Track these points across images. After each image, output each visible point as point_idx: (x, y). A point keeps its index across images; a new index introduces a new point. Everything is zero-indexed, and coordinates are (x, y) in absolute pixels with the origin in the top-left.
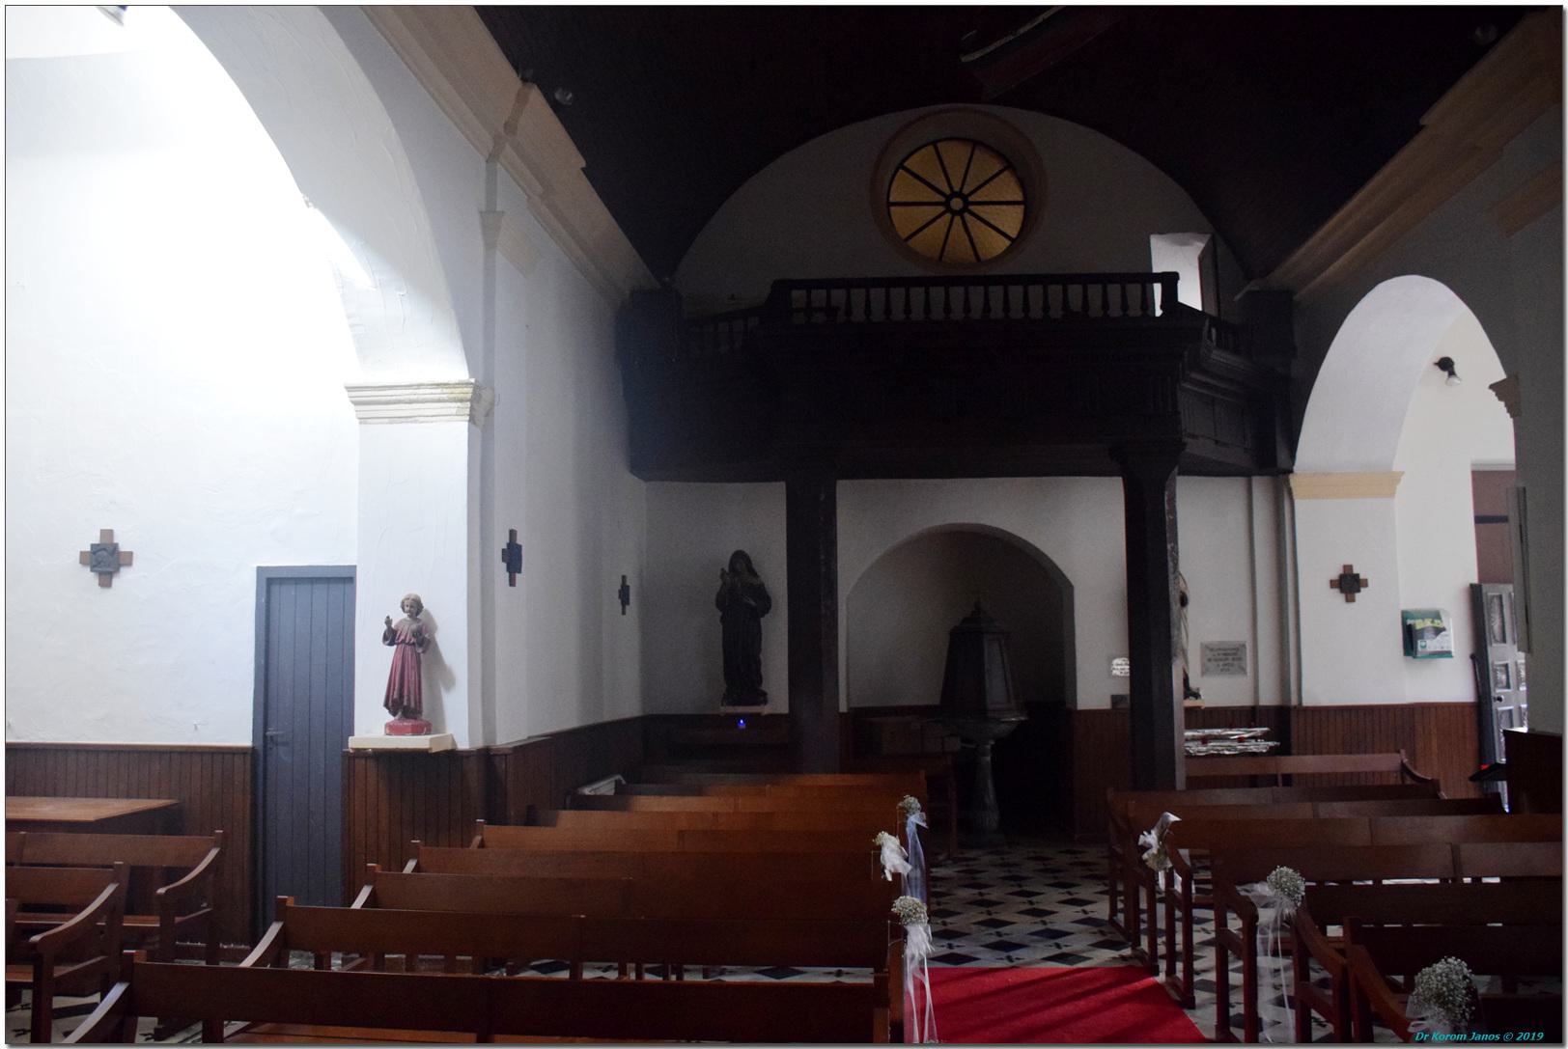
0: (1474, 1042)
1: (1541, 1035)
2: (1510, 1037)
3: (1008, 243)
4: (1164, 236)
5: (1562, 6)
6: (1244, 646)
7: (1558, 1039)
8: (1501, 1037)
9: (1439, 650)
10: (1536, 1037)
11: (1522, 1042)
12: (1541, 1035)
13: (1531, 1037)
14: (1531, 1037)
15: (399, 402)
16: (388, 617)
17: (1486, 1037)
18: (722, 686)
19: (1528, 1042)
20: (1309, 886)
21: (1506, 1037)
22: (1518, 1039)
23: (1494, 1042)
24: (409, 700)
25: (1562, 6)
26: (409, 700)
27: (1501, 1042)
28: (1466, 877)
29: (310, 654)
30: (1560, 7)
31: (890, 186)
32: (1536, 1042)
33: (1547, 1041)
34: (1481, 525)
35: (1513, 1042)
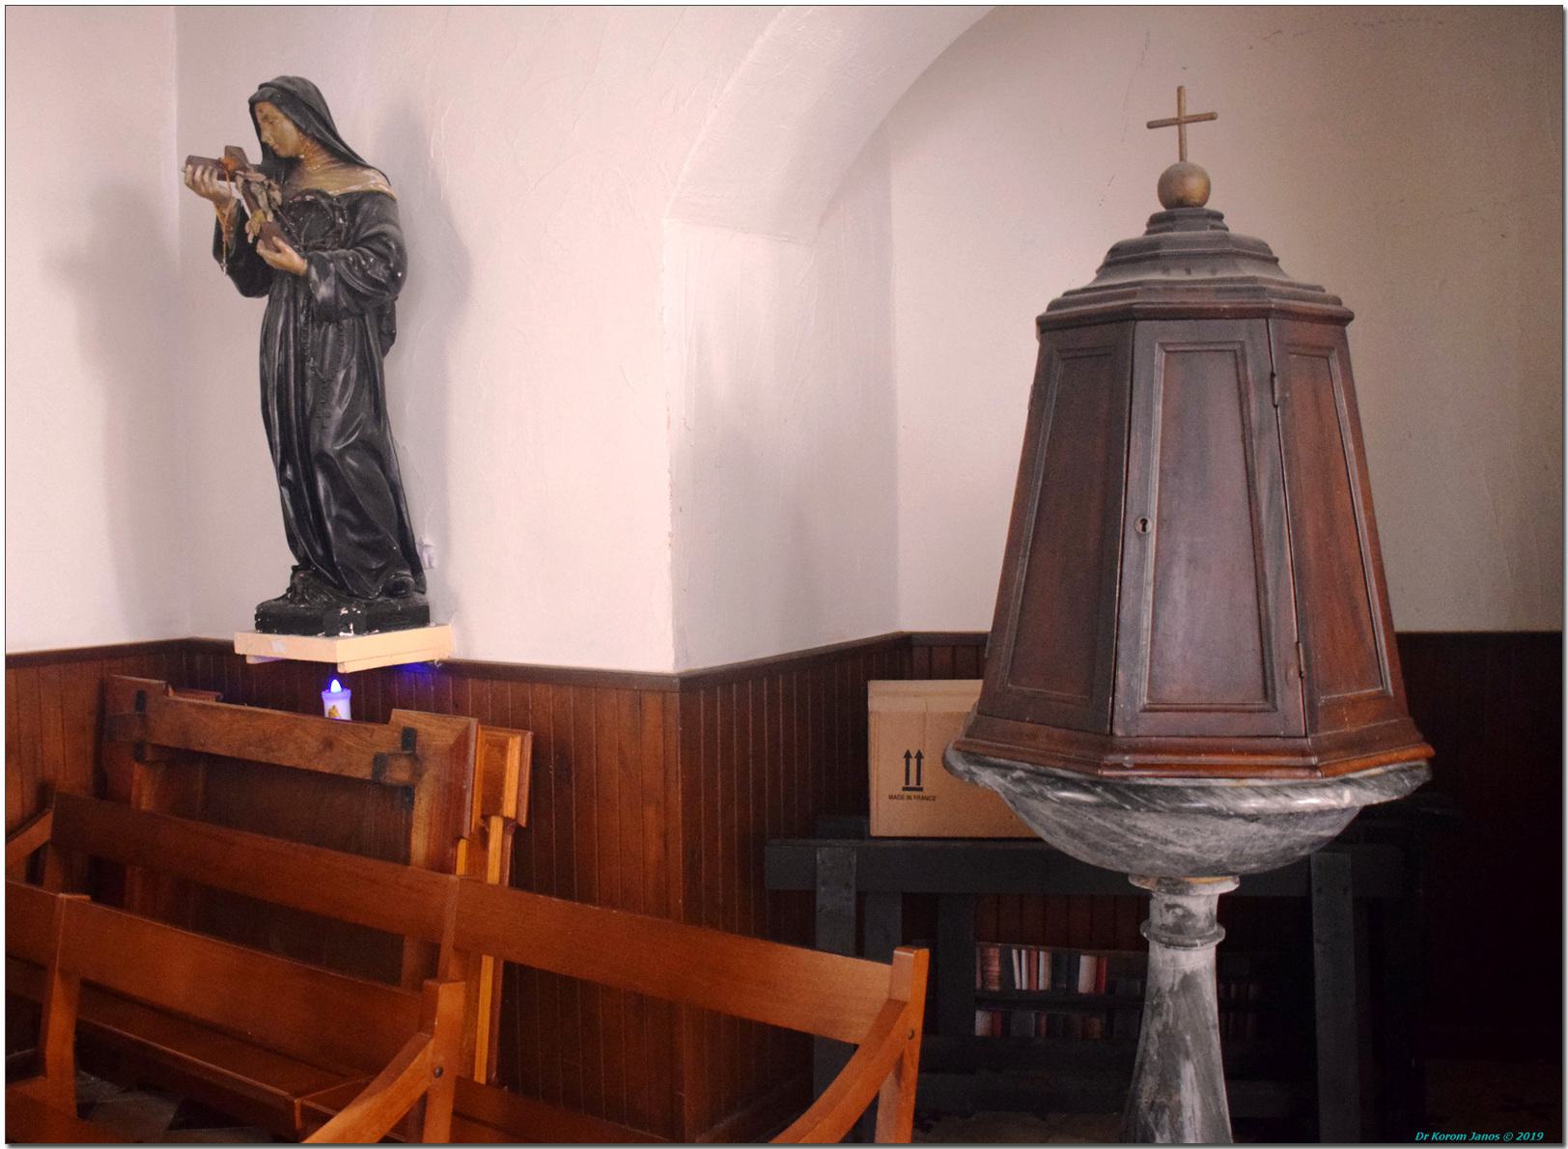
0: (1474, 1142)
1: (1541, 1136)
2: (1510, 1137)
4: (351, 1105)
6: (420, 617)
7: (1558, 1139)
8: (1501, 1137)
10: (1536, 1137)
11: (1522, 1142)
12: (1541, 1136)
13: (1531, 1137)
14: (1531, 1137)
16: (908, 752)
17: (1486, 1137)
18: (448, 1137)
19: (1529, 1142)
21: (1506, 1137)
22: (1518, 1139)
23: (1493, 1142)
24: (1415, 759)
26: (1415, 759)
27: (1501, 1142)
28: (973, 1026)
29: (475, 1121)
32: (1537, 1142)
33: (1546, 1141)
34: (425, 1137)
35: (1513, 1142)
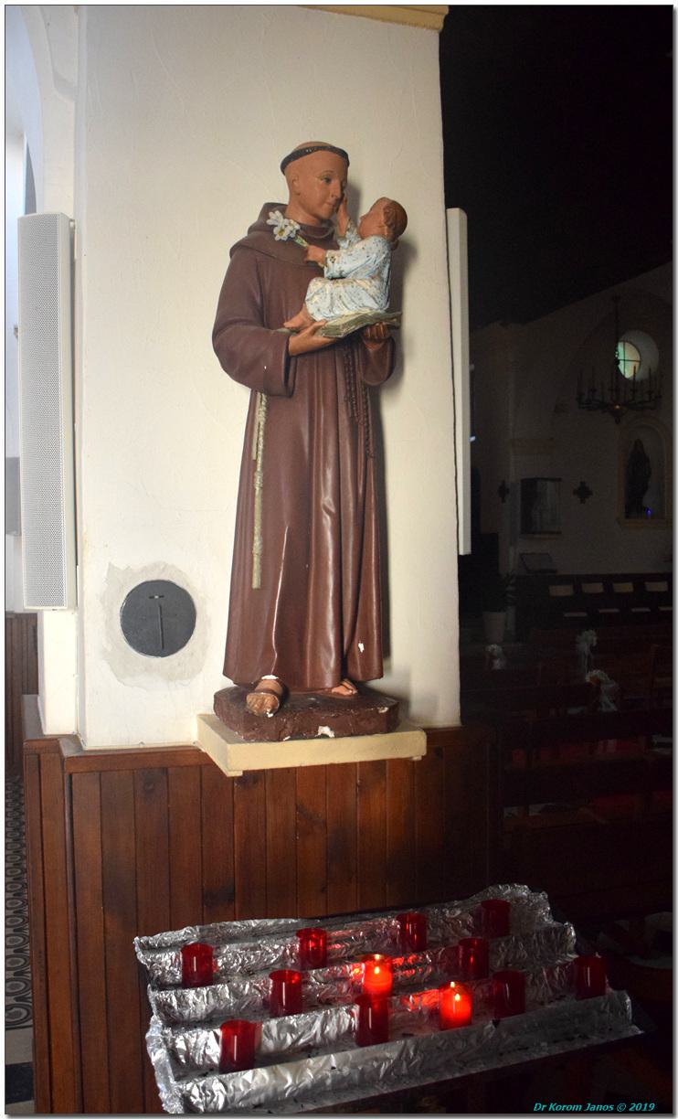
0: (589, 1112)
1: (652, 1106)
2: (623, 1107)
3: (31, 1029)
5: (672, 6)
7: (669, 1110)
8: (615, 1108)
9: (86, 652)
10: (648, 1108)
11: (635, 1112)
12: (652, 1106)
14: (643, 1107)
15: (76, 936)
17: (600, 1107)
19: (641, 1113)
20: (385, 765)
21: (620, 1108)
22: (631, 1109)
25: (672, 6)
27: (615, 1112)
30: (671, 7)
31: (51, 1095)
32: (648, 1112)
33: (659, 1111)
35: (626, 1112)
